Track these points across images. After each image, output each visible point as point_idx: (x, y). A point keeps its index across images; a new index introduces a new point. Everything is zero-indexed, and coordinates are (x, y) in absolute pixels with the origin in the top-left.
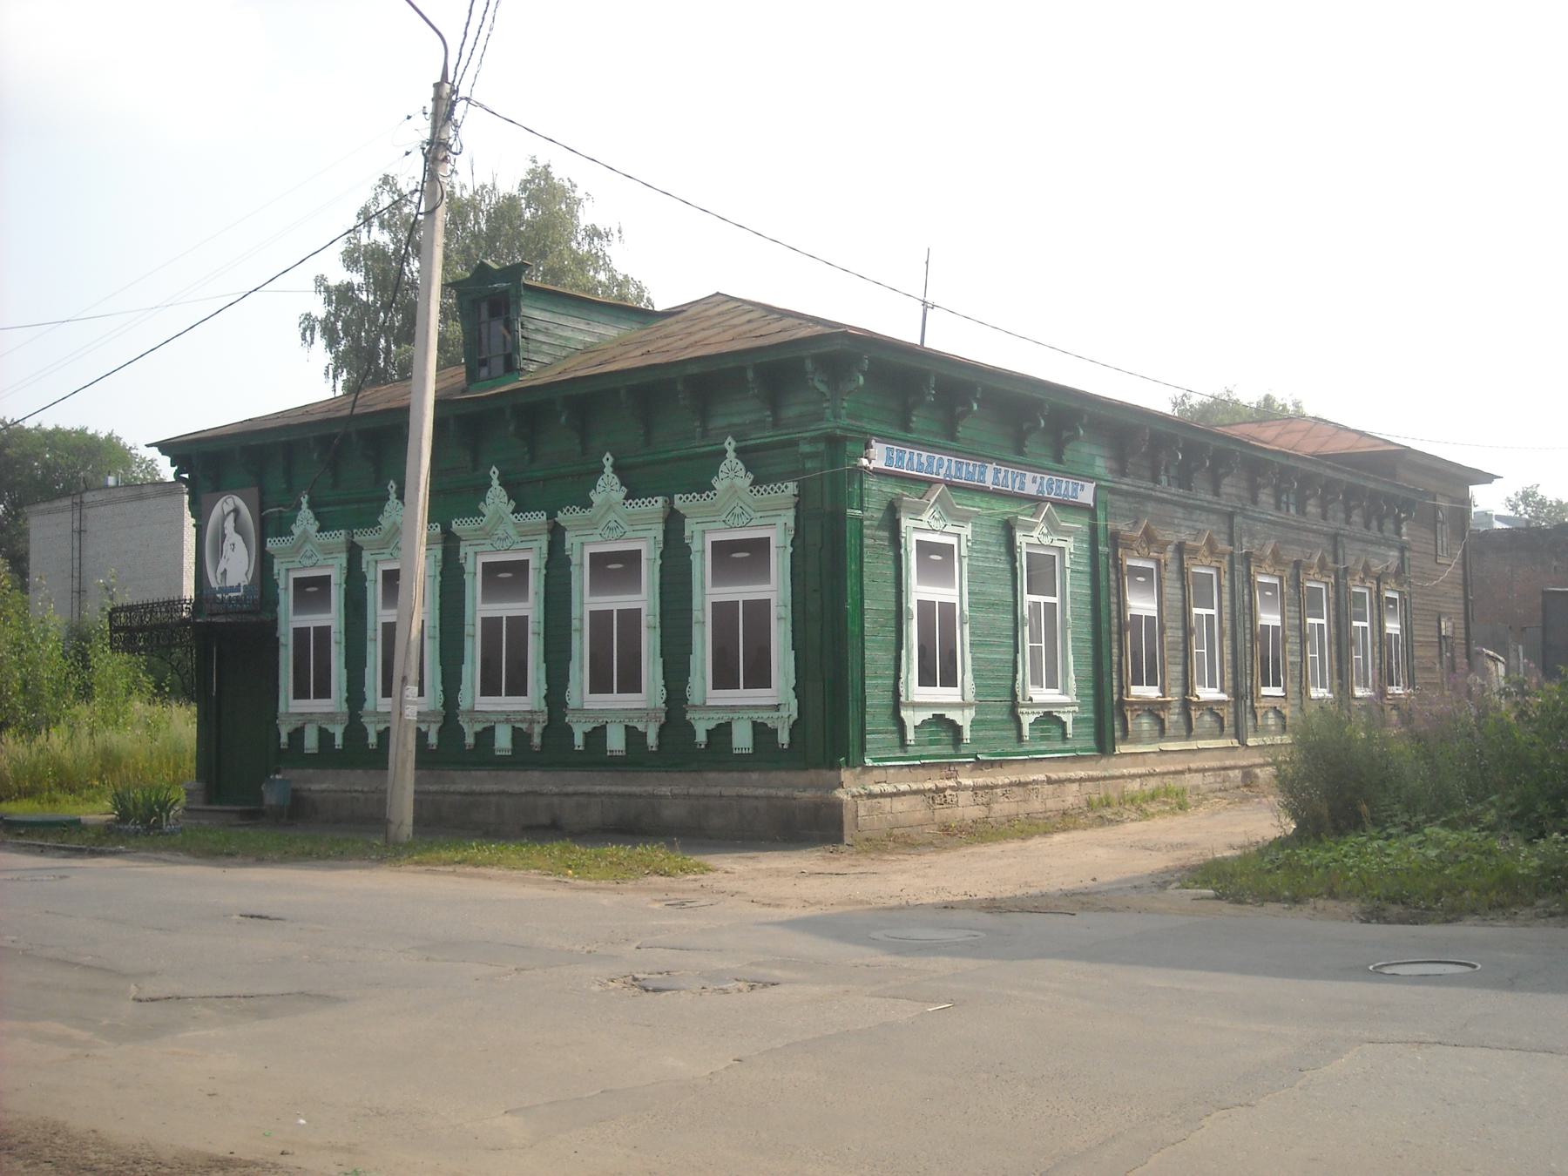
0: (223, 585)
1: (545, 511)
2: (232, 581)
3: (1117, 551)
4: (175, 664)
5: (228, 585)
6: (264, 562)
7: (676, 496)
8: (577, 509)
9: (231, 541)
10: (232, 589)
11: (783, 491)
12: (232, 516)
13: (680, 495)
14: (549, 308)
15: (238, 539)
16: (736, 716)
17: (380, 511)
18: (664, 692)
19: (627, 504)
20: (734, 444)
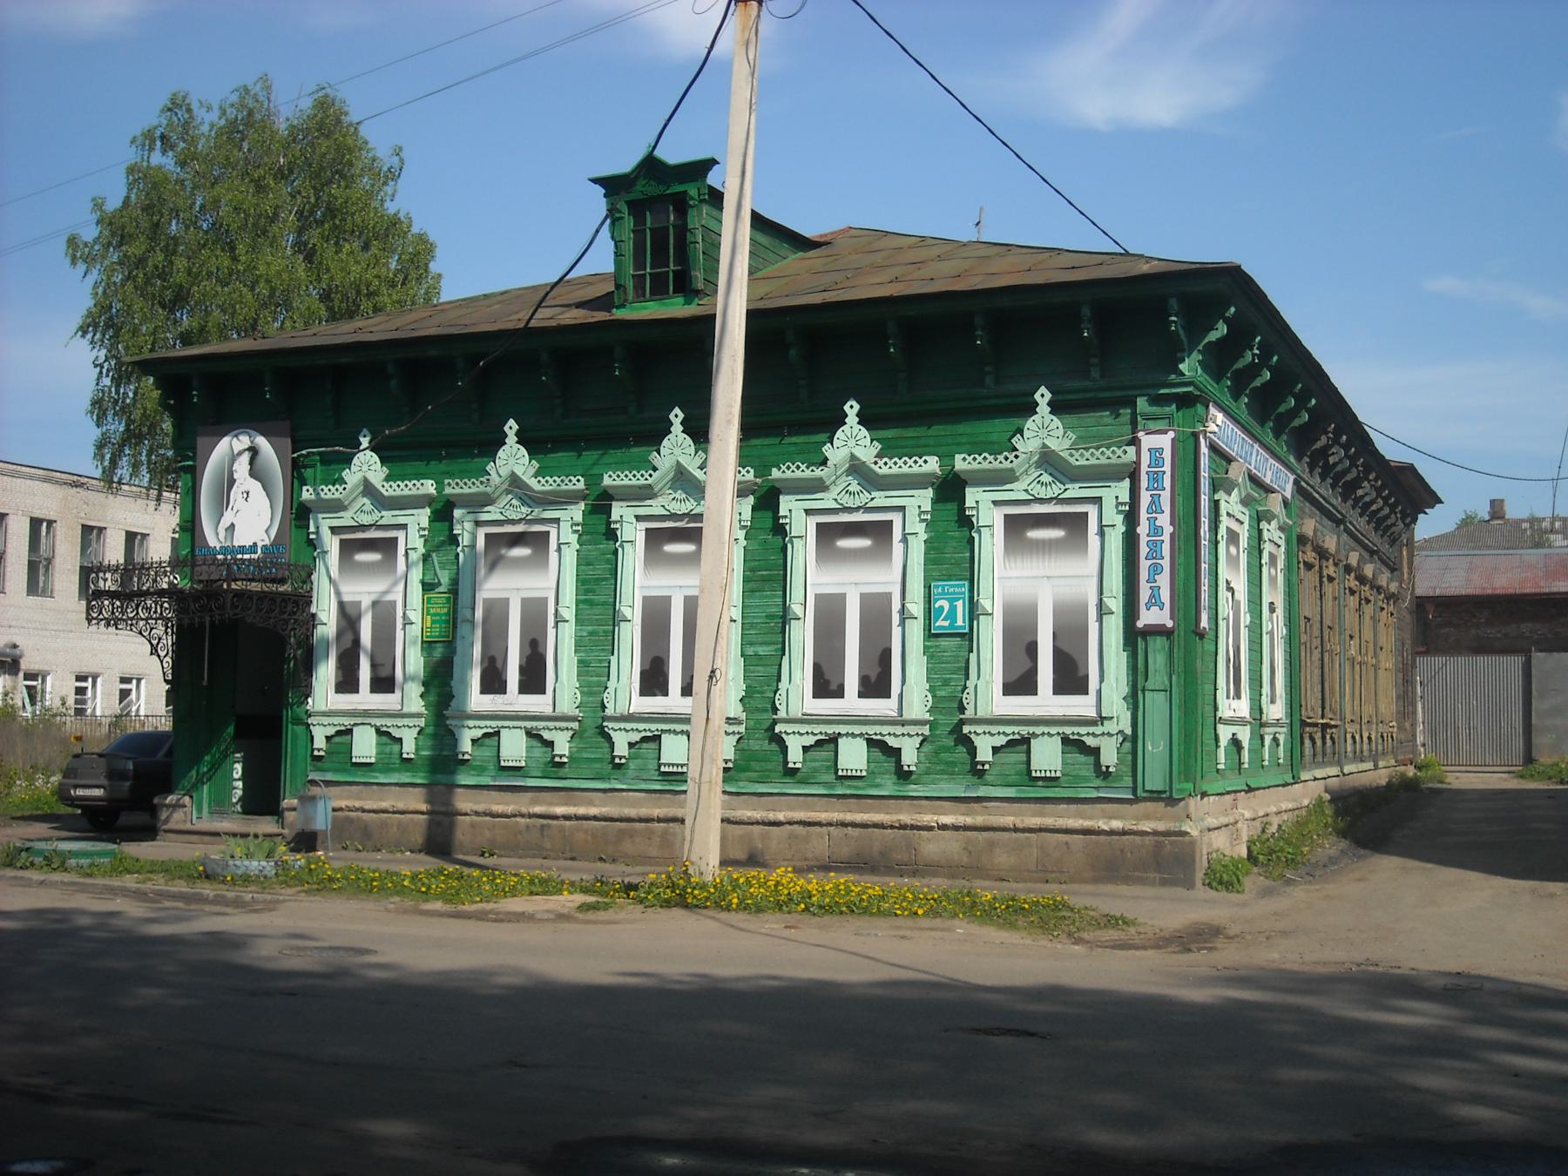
0: (228, 544)
1: (582, 476)
2: (242, 539)
3: (458, 860)
4: (155, 642)
5: (236, 544)
6: (299, 514)
7: (957, 456)
8: (803, 467)
9: (243, 489)
10: (242, 549)
11: (910, 466)
12: (246, 457)
13: (963, 456)
14: (1198, 266)
15: (255, 487)
16: (1038, 730)
17: (347, 460)
18: (930, 698)
19: (881, 463)
20: (1048, 396)
